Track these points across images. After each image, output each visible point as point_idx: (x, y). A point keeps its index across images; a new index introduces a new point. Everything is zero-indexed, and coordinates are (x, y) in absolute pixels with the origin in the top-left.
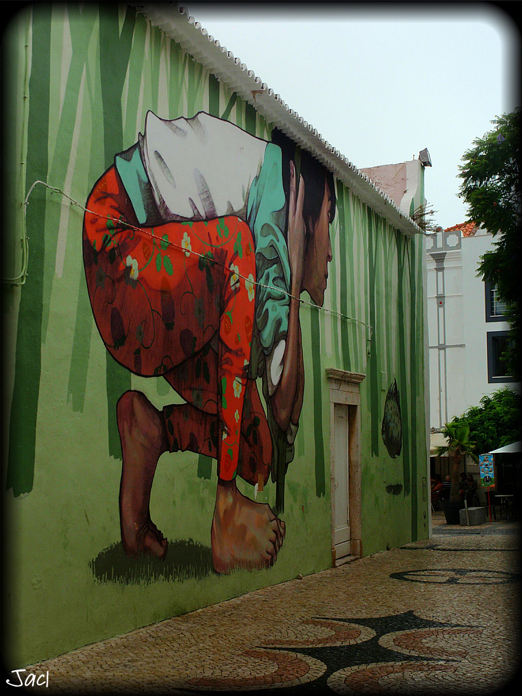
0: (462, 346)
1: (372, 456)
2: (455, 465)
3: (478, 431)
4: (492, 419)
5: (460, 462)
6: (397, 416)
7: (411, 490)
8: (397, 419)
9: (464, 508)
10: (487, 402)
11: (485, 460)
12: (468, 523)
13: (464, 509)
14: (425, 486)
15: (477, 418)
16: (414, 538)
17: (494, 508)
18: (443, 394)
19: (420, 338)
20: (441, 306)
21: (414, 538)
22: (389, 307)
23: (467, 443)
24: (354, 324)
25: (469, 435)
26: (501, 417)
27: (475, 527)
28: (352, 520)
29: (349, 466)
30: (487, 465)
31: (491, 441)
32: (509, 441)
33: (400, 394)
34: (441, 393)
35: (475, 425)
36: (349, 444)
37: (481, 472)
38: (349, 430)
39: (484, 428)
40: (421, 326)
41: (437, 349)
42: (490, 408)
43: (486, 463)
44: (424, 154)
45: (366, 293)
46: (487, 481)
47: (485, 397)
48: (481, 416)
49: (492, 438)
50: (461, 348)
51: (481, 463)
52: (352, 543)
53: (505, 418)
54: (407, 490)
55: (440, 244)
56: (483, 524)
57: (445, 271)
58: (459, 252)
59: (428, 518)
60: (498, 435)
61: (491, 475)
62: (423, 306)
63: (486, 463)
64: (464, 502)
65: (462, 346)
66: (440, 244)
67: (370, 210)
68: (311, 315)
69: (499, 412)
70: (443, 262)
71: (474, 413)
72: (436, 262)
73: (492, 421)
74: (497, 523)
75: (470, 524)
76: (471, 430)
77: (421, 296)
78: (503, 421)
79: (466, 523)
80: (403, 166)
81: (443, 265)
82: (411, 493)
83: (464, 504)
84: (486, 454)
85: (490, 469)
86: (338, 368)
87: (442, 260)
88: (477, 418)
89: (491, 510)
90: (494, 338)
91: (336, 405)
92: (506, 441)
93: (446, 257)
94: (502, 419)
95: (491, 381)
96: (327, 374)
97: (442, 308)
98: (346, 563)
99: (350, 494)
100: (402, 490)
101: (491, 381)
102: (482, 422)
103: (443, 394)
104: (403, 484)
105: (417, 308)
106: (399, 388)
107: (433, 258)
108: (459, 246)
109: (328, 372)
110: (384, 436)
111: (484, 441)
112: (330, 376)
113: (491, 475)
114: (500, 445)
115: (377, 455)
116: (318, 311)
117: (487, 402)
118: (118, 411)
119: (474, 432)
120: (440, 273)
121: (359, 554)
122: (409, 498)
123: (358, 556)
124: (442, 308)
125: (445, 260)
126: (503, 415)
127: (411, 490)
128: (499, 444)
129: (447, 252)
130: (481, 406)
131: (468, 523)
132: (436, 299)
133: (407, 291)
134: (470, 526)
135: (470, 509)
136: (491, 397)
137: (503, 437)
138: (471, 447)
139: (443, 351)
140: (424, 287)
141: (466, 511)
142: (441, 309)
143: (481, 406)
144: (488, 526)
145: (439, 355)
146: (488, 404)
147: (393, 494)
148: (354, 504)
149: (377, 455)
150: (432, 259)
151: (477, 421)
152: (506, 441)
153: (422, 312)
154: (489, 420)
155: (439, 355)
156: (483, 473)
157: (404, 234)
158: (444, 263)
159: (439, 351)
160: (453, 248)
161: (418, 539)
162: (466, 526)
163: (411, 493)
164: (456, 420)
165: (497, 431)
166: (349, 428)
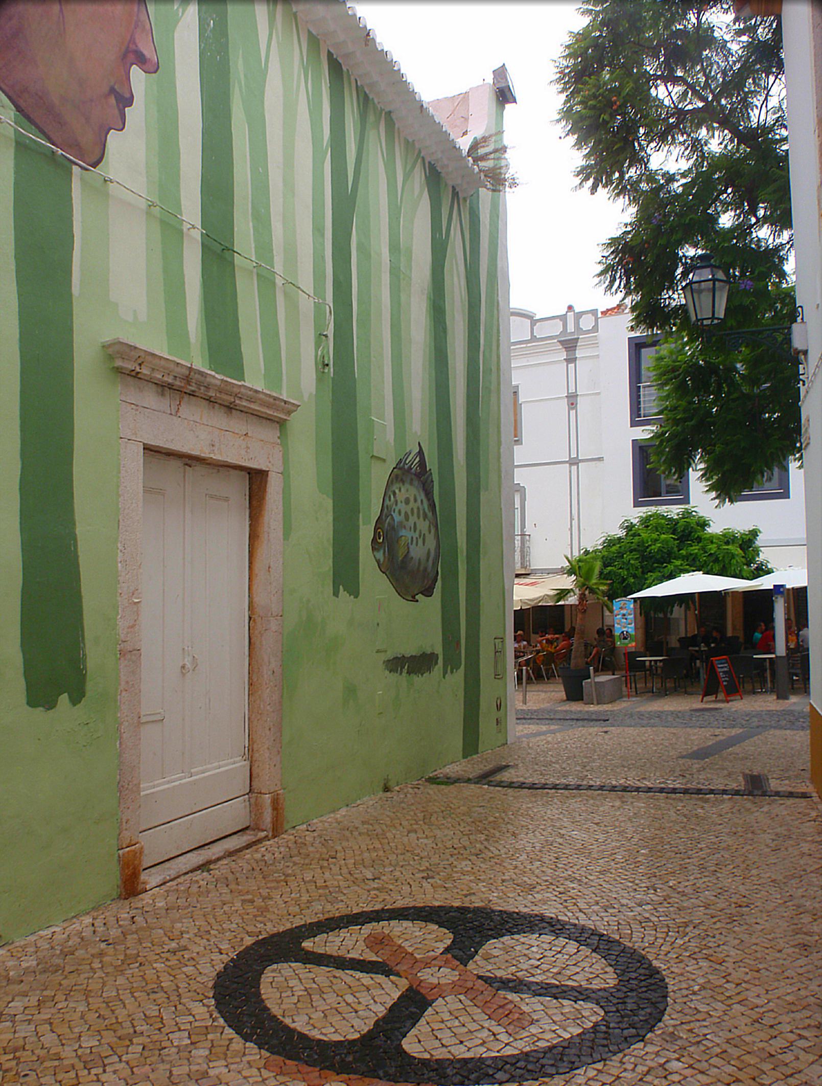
0: (600, 459)
1: (336, 594)
2: (580, 615)
3: (615, 566)
4: (635, 550)
5: (585, 610)
6: (425, 516)
7: (463, 662)
8: (423, 525)
9: (589, 678)
10: (630, 528)
11: (621, 608)
12: (595, 702)
13: (589, 680)
14: (499, 653)
15: (614, 549)
16: (471, 746)
17: (635, 676)
18: (575, 522)
19: (492, 388)
20: (573, 409)
21: (471, 746)
22: (403, 298)
23: (596, 584)
24: (266, 280)
25: (601, 573)
26: (647, 547)
27: (605, 706)
28: (255, 746)
29: (250, 618)
30: (624, 615)
31: (633, 580)
32: (658, 580)
33: (435, 477)
34: (573, 522)
35: (611, 559)
36: (251, 563)
37: (616, 625)
38: (251, 530)
39: (624, 563)
40: (494, 369)
41: (568, 465)
42: (631, 535)
43: (624, 612)
44: (501, 73)
45: (318, 230)
46: (625, 638)
47: (626, 520)
48: (620, 547)
49: (635, 576)
50: (598, 463)
51: (615, 612)
52: (253, 801)
53: (653, 547)
54: (451, 664)
55: (571, 328)
56: (617, 702)
57: (577, 362)
58: (596, 336)
59: (506, 707)
60: (643, 573)
61: (630, 630)
62: (499, 336)
63: (624, 612)
64: (589, 670)
65: (600, 459)
66: (571, 328)
67: (335, 67)
68: (17, 165)
69: (645, 540)
70: (575, 350)
71: (610, 542)
72: (567, 351)
73: (634, 553)
74: (638, 699)
75: (597, 700)
76: (606, 565)
77: (496, 316)
78: (650, 553)
79: (592, 699)
80: (464, 98)
81: (575, 355)
82: (463, 666)
83: (589, 672)
84: (624, 599)
85: (629, 621)
86: (170, 354)
87: (574, 348)
88: (614, 549)
89: (631, 679)
90: (641, 448)
91: (147, 448)
92: (653, 581)
93: (579, 344)
94: (648, 550)
95: (637, 504)
96: (111, 358)
97: (574, 411)
98: (198, 868)
99: (250, 684)
100: (436, 663)
101: (637, 504)
102: (620, 555)
103: (575, 522)
104: (439, 650)
105: (485, 333)
106: (432, 464)
107: (562, 345)
108: (595, 328)
109: (110, 351)
110: (380, 555)
111: (624, 580)
112: (119, 363)
113: (631, 629)
114: (645, 587)
115: (355, 592)
116: (71, 173)
117: (630, 528)
118: (688, 625)
119: (609, 568)
120: (571, 366)
121: (270, 826)
122: (458, 678)
123: (263, 834)
124: (574, 411)
125: (578, 348)
126: (650, 543)
127: (463, 662)
128: (645, 584)
129: (581, 337)
130: (621, 533)
131: (595, 702)
132: (566, 400)
133: (456, 291)
134: (598, 704)
135: (598, 679)
136: (635, 521)
137: (649, 574)
138: (601, 588)
139: (576, 467)
140: (501, 303)
141: (593, 683)
142: (573, 413)
143: (621, 533)
144: (624, 705)
145: (570, 472)
146: (631, 530)
147: (409, 673)
148: (259, 707)
149: (355, 592)
150: (561, 347)
151: (614, 553)
152: (653, 581)
153: (498, 346)
154: (631, 551)
155: (570, 472)
156: (619, 626)
157: (451, 183)
158: (577, 352)
159: (570, 467)
160: (588, 332)
161: (480, 750)
162: (592, 704)
163: (463, 666)
164: (587, 552)
165: (642, 567)
166: (250, 525)
